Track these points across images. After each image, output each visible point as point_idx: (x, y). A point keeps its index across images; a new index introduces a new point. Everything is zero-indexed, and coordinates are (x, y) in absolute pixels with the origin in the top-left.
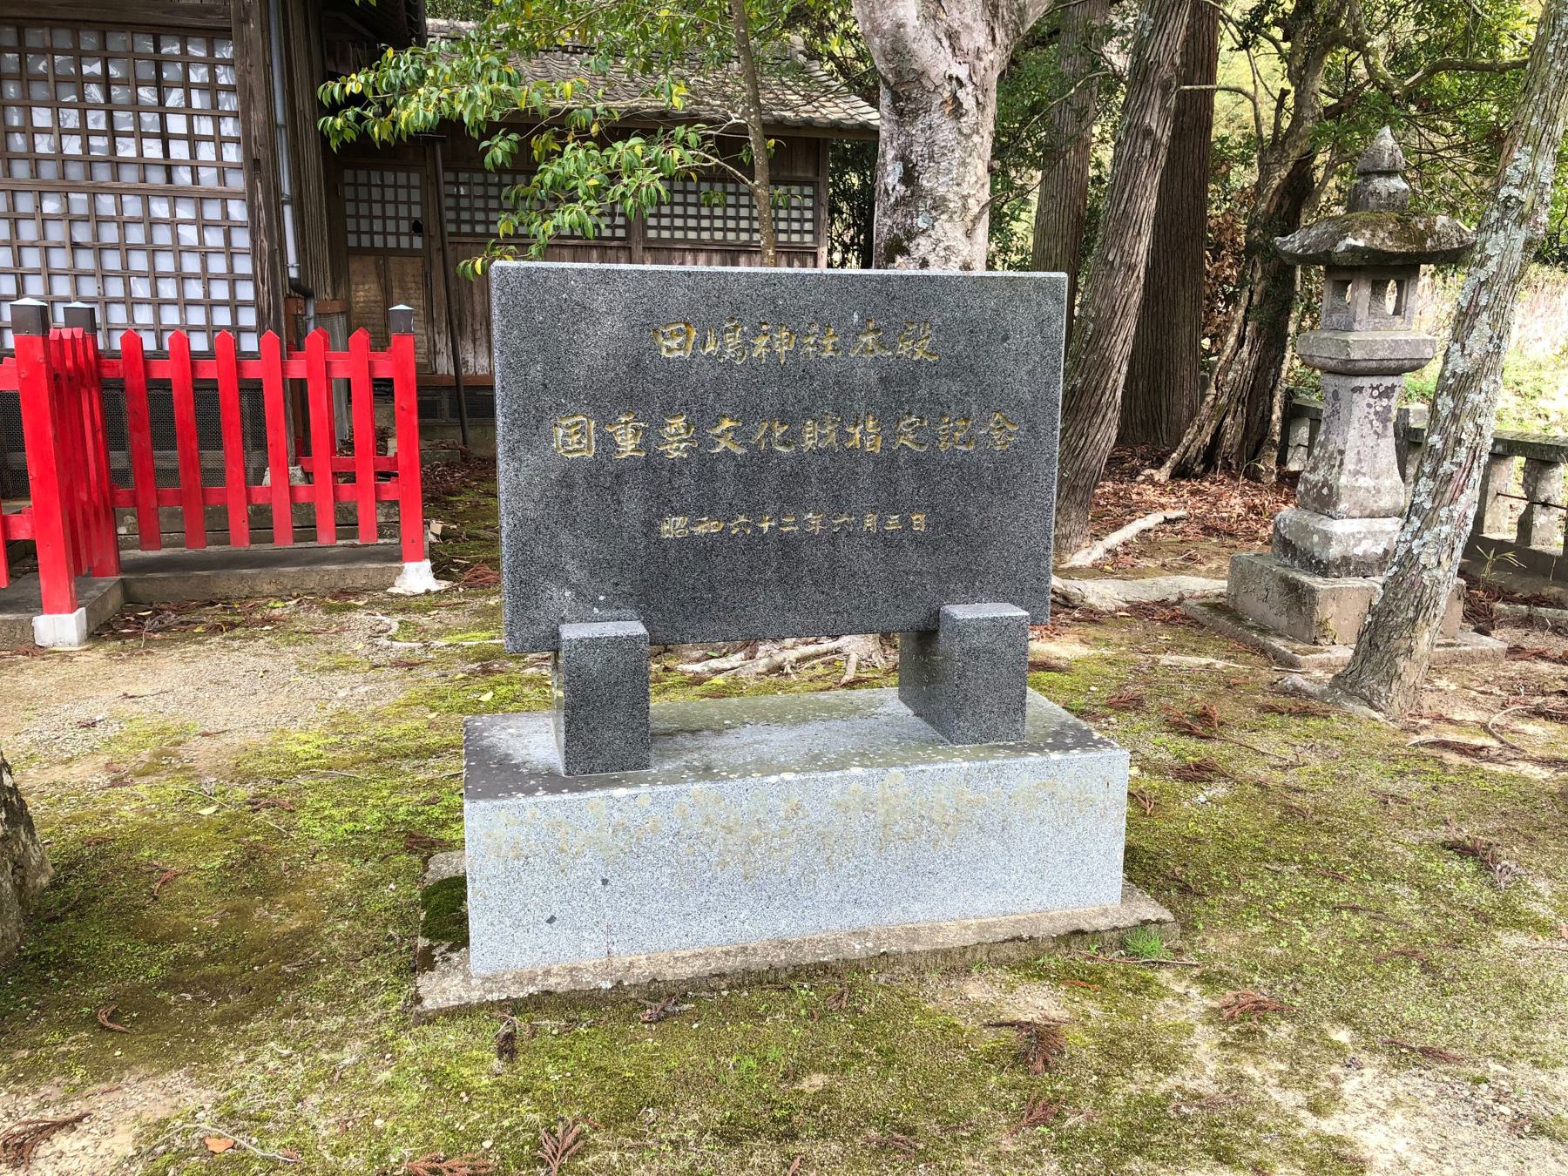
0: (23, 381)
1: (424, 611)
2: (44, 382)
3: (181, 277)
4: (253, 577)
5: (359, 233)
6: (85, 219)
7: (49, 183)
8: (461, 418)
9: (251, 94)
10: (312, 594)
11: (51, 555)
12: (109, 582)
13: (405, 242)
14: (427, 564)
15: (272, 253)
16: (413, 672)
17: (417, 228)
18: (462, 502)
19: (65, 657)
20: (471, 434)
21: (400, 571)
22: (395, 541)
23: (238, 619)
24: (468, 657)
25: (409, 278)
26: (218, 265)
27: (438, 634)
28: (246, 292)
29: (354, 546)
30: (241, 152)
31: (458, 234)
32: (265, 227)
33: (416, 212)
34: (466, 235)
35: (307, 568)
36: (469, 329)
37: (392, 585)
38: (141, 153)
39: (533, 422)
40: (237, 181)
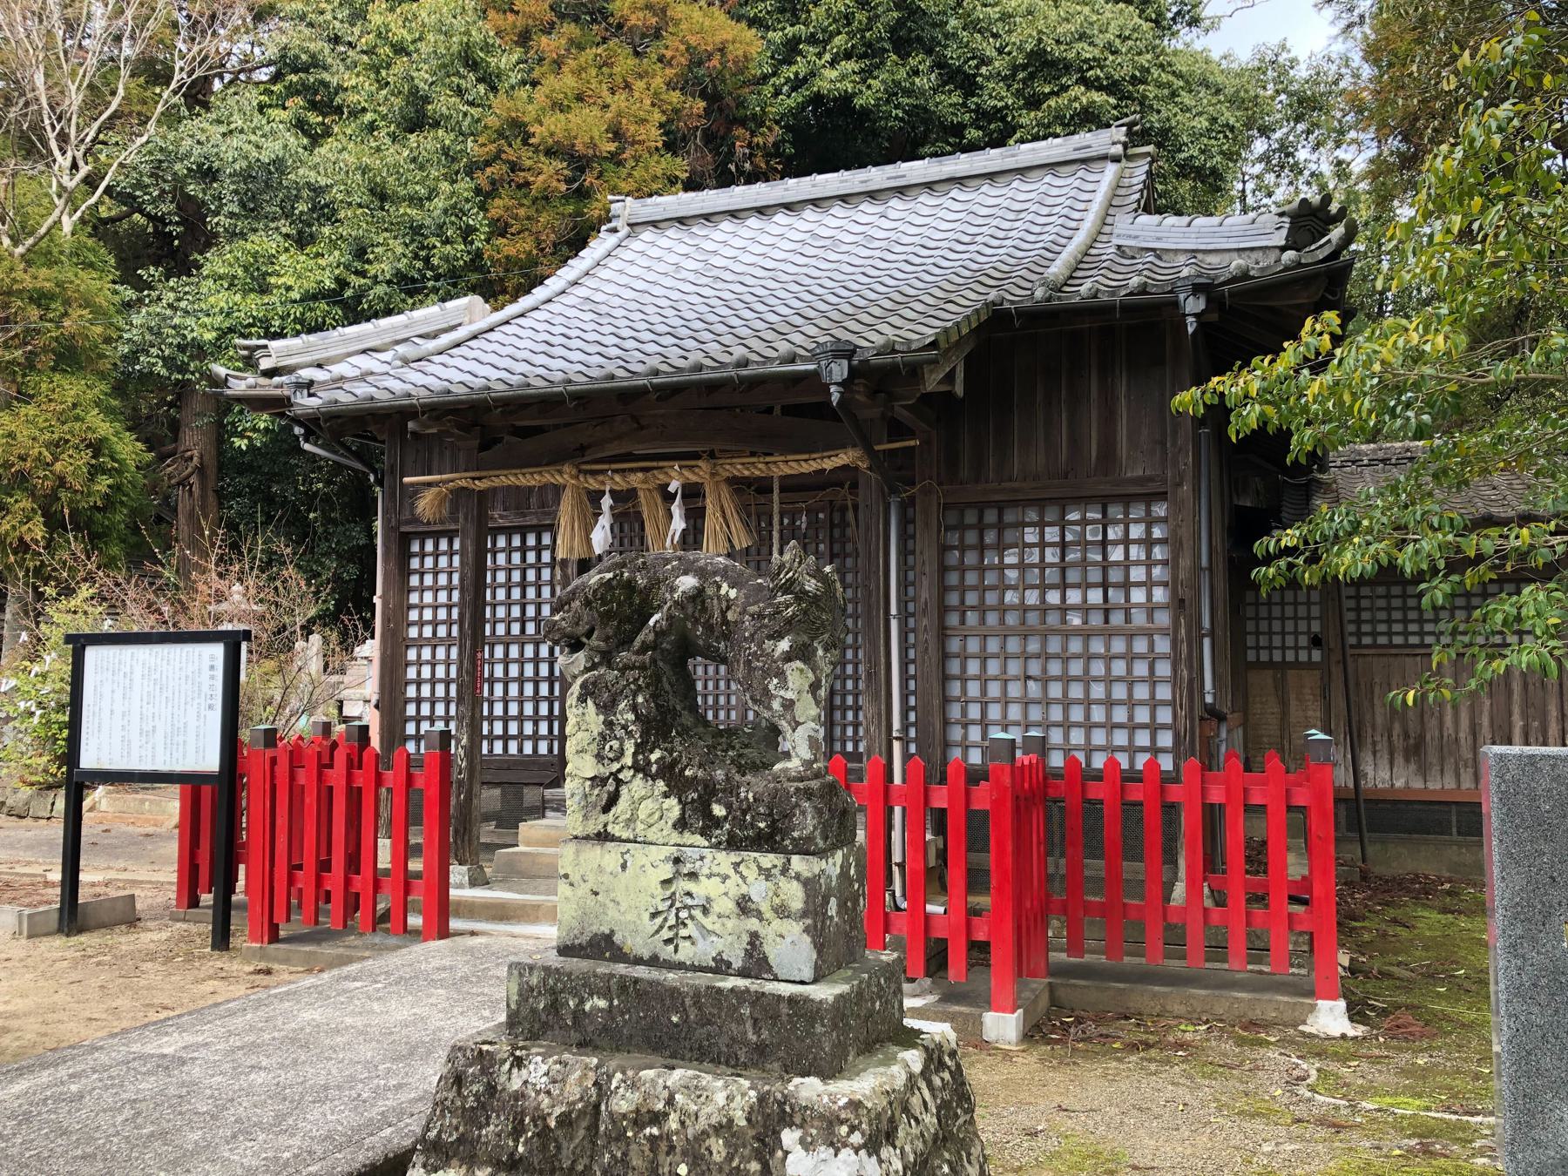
0: (993, 802)
1: (1344, 1059)
2: (1009, 804)
3: (1109, 703)
4: (1165, 995)
5: (1258, 648)
6: (1038, 656)
7: (1011, 628)
8: (1360, 831)
9: (1181, 543)
10: (1221, 1021)
11: (1001, 955)
12: (1039, 984)
13: (1303, 656)
14: (1342, 1004)
15: (1191, 681)
16: (1341, 1136)
17: (1316, 642)
18: (1369, 929)
19: (1007, 1056)
20: (1370, 850)
21: (1313, 1008)
22: (1303, 971)
23: (1152, 1039)
24: (1403, 1129)
25: (1307, 691)
26: (1141, 692)
27: (1364, 1093)
28: (1165, 716)
29: (1261, 972)
30: (1168, 593)
31: (1359, 645)
32: (1186, 661)
33: (1316, 627)
34: (1367, 646)
35: (1217, 992)
36: (1369, 740)
37: (1304, 1023)
38: (1085, 600)
39: (1540, 918)
40: (1163, 619)
